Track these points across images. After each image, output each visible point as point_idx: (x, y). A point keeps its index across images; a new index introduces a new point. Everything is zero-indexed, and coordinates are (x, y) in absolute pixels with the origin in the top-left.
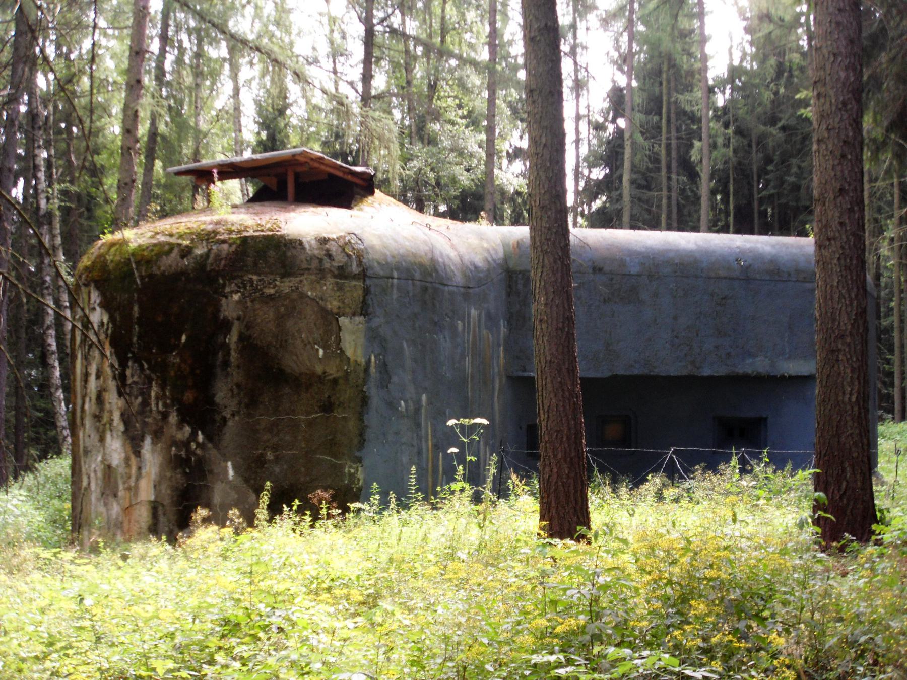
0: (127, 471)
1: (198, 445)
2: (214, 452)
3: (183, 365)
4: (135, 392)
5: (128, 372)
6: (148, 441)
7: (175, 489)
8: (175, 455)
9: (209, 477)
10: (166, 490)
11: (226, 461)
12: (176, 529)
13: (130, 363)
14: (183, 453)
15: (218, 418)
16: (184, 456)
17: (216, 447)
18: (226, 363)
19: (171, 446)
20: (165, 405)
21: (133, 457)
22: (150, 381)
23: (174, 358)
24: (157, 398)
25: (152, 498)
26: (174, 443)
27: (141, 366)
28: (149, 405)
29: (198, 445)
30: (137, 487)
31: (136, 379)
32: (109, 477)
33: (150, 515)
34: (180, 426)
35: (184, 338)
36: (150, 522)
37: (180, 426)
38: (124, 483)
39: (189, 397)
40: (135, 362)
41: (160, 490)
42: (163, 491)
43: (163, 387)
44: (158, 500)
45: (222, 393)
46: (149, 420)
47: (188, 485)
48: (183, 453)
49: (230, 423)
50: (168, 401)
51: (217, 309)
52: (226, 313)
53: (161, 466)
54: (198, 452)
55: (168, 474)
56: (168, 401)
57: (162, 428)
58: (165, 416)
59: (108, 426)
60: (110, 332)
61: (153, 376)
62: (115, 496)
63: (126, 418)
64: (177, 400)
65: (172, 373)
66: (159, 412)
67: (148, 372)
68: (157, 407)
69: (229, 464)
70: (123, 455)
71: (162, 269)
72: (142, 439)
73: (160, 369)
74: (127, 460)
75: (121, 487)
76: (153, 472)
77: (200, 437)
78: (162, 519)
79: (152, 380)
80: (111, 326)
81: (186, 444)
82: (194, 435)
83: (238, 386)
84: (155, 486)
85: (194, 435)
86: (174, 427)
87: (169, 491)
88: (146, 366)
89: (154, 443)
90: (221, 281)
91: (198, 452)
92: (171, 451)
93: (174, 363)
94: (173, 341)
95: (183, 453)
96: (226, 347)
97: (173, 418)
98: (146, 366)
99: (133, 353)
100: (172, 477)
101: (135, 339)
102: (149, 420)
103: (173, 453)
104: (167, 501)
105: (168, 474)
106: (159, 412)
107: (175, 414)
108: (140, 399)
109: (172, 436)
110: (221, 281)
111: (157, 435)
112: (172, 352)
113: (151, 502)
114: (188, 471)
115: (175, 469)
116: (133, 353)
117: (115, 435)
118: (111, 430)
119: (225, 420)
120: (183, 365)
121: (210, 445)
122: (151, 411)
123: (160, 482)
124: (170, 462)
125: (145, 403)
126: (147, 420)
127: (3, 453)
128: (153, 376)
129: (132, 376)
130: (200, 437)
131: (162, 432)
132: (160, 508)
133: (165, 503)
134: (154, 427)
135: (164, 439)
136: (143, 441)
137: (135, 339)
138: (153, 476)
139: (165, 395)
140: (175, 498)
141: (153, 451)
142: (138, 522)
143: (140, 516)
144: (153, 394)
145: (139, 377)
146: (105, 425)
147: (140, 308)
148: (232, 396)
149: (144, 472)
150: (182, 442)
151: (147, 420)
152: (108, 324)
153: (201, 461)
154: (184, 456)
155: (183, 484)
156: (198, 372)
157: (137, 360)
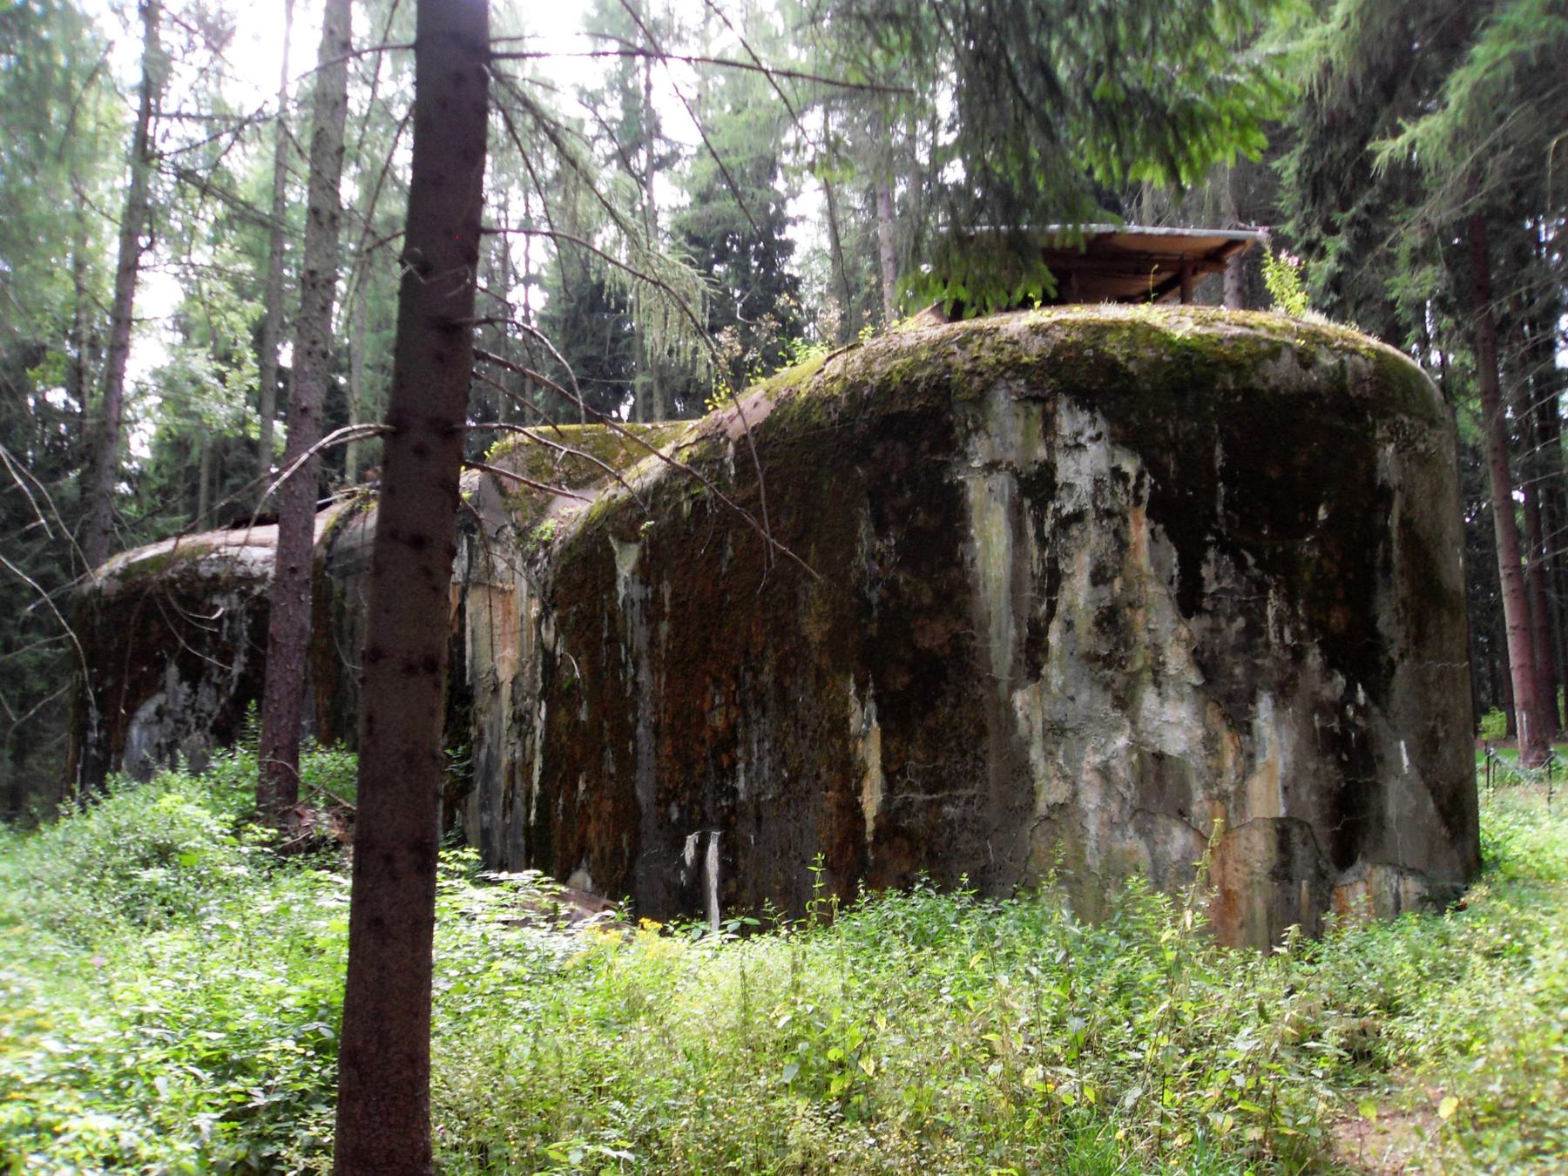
0: (1211, 762)
1: (1358, 709)
2: (1381, 722)
3: (1326, 563)
4: (1227, 605)
5: (1206, 572)
6: (1264, 707)
7: (1324, 792)
8: (1323, 729)
9: (1379, 768)
10: (1307, 796)
11: (1398, 739)
12: (1333, 871)
13: (1211, 554)
14: (1335, 725)
15: (1383, 660)
16: (1337, 730)
17: (1384, 713)
18: (1387, 566)
19: (1313, 712)
20: (1296, 634)
21: (1226, 736)
22: (1263, 588)
23: (1307, 547)
24: (1279, 620)
25: (1282, 812)
26: (1319, 706)
27: (1241, 565)
28: (1262, 632)
29: (1358, 709)
30: (1241, 793)
31: (1227, 583)
32: (1160, 778)
33: (1274, 846)
34: (1327, 676)
35: (1322, 514)
36: (1275, 860)
37: (1327, 676)
38: (1207, 786)
39: (1337, 619)
40: (1222, 551)
41: (1298, 797)
42: (1304, 798)
43: (1291, 600)
44: (1296, 815)
45: (1388, 620)
46: (1266, 663)
47: (1348, 783)
48: (1335, 725)
49: (1399, 671)
50: (1303, 627)
51: (1372, 469)
52: (1385, 476)
53: (1296, 750)
54: (1360, 722)
55: (1312, 765)
56: (1303, 627)
57: (1293, 677)
58: (1298, 655)
59: (1147, 676)
60: (1145, 493)
61: (1269, 579)
62: (1182, 813)
63: (1205, 661)
64: (1316, 626)
65: (1307, 576)
66: (1285, 647)
67: (1256, 572)
68: (1282, 637)
69: (1402, 744)
70: (1199, 732)
71: (1272, 382)
72: (1252, 698)
73: (1284, 568)
74: (1210, 743)
75: (1199, 795)
76: (1281, 762)
77: (1361, 696)
78: (1300, 852)
79: (1268, 586)
80: (1148, 479)
81: (1338, 708)
82: (1350, 690)
83: (1404, 604)
84: (1285, 789)
85: (1350, 690)
86: (1317, 677)
87: (1314, 798)
88: (1251, 561)
89: (1278, 706)
90: (1370, 419)
91: (1360, 722)
92: (1312, 723)
93: (1309, 559)
94: (1301, 516)
95: (1335, 725)
96: (1385, 531)
97: (1314, 659)
98: (1251, 561)
99: (1217, 533)
100: (1318, 769)
101: (1219, 508)
102: (1266, 663)
103: (1317, 724)
104: (1313, 817)
105: (1312, 765)
106: (1285, 647)
107: (1317, 651)
108: (1240, 622)
109: (1314, 693)
110: (1370, 419)
111: (1284, 692)
112: (1302, 537)
113: (1279, 820)
114: (1345, 757)
115: (1322, 754)
116: (1217, 533)
117: (1172, 693)
118: (1157, 684)
119: (1392, 666)
120: (1326, 563)
121: (1375, 710)
122: (1267, 645)
123: (1295, 781)
124: (1314, 741)
125: (1254, 629)
126: (1259, 662)
127: (23, 746)
128: (1269, 579)
129: (1218, 578)
130: (1361, 696)
131: (1295, 685)
132: (1296, 830)
133: (1310, 820)
134: (1276, 677)
135: (1298, 698)
136: (1254, 703)
137: (1219, 508)
138: (1280, 770)
139: (1294, 613)
140: (1328, 811)
141: (1278, 722)
142: (1245, 862)
143: (1251, 849)
144: (1270, 612)
145: (1237, 580)
146: (1135, 677)
147: (1226, 449)
148: (1399, 622)
149: (1260, 762)
150: (1333, 704)
151: (1259, 662)
152: (1140, 476)
153: (1365, 739)
154: (1337, 730)
155: (1338, 784)
156: (1350, 576)
157: (1224, 547)
